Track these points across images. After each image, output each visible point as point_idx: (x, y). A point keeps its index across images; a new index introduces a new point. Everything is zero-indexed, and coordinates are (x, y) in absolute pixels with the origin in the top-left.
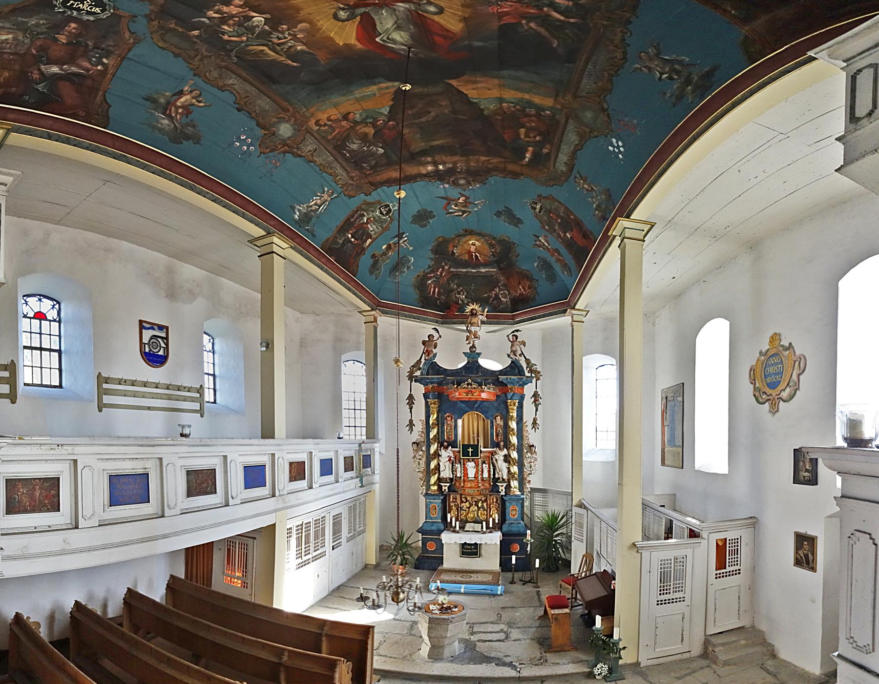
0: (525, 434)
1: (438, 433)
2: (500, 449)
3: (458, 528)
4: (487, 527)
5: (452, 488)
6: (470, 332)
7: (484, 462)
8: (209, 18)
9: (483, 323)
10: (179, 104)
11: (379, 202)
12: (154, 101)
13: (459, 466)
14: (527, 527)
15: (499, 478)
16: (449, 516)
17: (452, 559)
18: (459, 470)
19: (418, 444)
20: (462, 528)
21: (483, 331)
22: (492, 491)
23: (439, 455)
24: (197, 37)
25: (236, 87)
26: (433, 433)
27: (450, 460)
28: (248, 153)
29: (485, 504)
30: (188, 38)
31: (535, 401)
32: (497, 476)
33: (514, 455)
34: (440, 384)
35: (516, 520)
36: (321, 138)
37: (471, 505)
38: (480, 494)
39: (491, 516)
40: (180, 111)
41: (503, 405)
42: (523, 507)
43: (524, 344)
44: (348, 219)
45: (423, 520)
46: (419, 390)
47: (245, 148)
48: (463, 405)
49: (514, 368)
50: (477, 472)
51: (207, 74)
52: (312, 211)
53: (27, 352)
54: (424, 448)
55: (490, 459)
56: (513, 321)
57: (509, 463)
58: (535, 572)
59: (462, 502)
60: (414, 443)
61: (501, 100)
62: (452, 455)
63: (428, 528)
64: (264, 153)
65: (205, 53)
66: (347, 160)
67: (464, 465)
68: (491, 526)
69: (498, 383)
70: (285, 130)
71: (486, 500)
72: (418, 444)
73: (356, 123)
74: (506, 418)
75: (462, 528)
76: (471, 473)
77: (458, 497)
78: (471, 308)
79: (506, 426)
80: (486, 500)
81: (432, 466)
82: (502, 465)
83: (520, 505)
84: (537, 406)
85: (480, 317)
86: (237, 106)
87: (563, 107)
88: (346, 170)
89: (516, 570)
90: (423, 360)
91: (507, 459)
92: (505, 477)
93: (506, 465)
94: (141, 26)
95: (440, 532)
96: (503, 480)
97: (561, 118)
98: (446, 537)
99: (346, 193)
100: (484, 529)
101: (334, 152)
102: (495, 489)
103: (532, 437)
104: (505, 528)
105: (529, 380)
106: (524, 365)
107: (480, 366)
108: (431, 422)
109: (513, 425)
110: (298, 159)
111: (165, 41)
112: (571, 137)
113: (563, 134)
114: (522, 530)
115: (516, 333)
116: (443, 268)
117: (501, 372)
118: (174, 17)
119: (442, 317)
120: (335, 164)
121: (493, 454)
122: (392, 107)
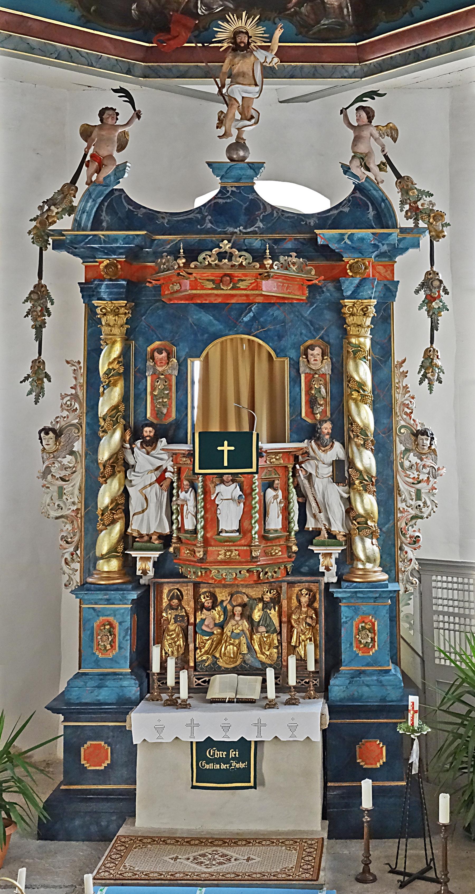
0: (398, 397)
1: (125, 398)
2: (321, 444)
3: (184, 693)
4: (281, 687)
5: (168, 566)
6: (228, 100)
7: (270, 485)
9: (269, 73)
13: (190, 496)
14: (409, 684)
15: (317, 532)
16: (156, 652)
17: (165, 797)
18: (190, 507)
19: (58, 434)
20: (199, 690)
21: (268, 97)
22: (296, 571)
23: (127, 466)
26: (110, 399)
27: (160, 480)
29: (273, 614)
31: (430, 300)
32: (311, 525)
33: (367, 460)
34: (134, 254)
35: (375, 661)
37: (228, 616)
38: (258, 582)
39: (292, 649)
41: (328, 315)
42: (394, 618)
43: (393, 133)
45: (70, 667)
46: (67, 271)
48: (206, 318)
49: (364, 206)
50: (247, 515)
54: (78, 446)
55: (291, 471)
56: (359, 62)
57: (351, 484)
58: (437, 840)
59: (199, 607)
60: (46, 431)
62: (169, 465)
63: (87, 695)
67: (206, 492)
68: (292, 681)
69: (313, 250)
71: (276, 601)
72: (58, 434)
74: (339, 354)
75: (199, 690)
76: (229, 517)
77: (188, 592)
78: (231, 28)
79: (339, 376)
80: (276, 601)
81: (105, 497)
82: (328, 492)
83: (384, 612)
84: (434, 317)
85: (261, 55)
89: (379, 833)
90: (82, 185)
91: (343, 472)
92: (337, 528)
93: (341, 490)
95: (125, 707)
96: (332, 536)
98: (144, 724)
100: (271, 693)
102: (304, 563)
103: (425, 406)
104: (338, 687)
105: (409, 240)
106: (394, 196)
107: (257, 204)
108: (103, 368)
109: (363, 372)
114: (394, 695)
115: (369, 103)
117: (324, 220)
119: (148, 55)
121: (297, 458)
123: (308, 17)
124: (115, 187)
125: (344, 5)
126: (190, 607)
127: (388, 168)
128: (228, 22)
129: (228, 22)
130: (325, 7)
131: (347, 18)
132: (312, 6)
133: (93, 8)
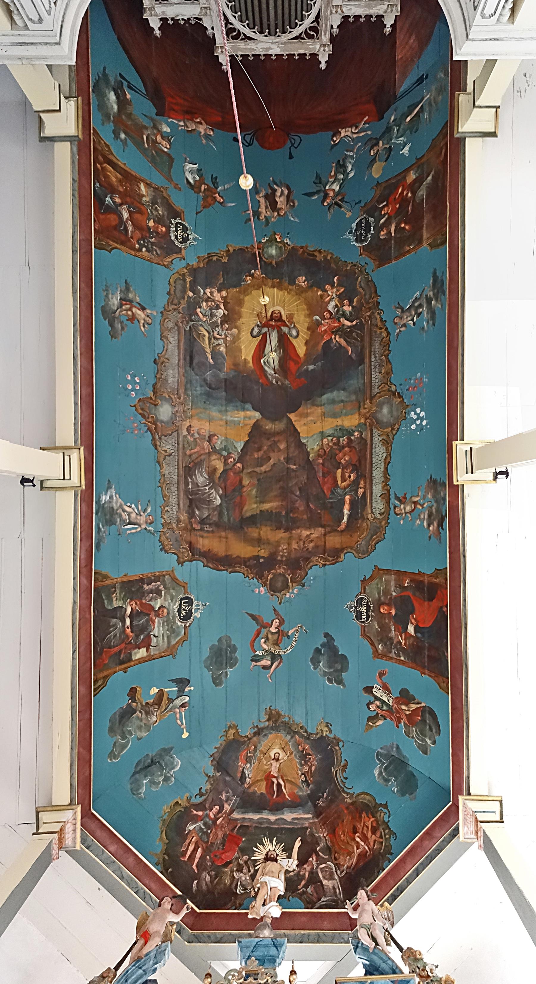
8: (205, 293)
10: (134, 310)
11: (184, 586)
12: (127, 289)
24: (189, 297)
25: (170, 346)
28: (127, 393)
30: (184, 291)
36: (182, 446)
40: (130, 313)
44: (142, 581)
47: (130, 387)
51: (166, 320)
52: (121, 516)
53: (74, 95)
61: (322, 435)
64: (136, 410)
65: (180, 308)
66: (187, 492)
70: (165, 412)
73: (214, 450)
86: (157, 358)
87: (366, 419)
88: (179, 505)
94: (179, 265)
97: (366, 434)
99: (163, 538)
101: (182, 473)
110: (153, 447)
111: (175, 282)
112: (379, 452)
113: (371, 454)
116: (222, 808)
118: (195, 278)
120: (174, 488)
122: (246, 443)
123: (312, 895)
124: (149, 978)
125: (336, 886)
126: (111, 492)
127: (392, 943)
128: (263, 845)
129: (263, 845)
130: (323, 889)
131: (339, 896)
132: (314, 888)
133: (170, 870)
